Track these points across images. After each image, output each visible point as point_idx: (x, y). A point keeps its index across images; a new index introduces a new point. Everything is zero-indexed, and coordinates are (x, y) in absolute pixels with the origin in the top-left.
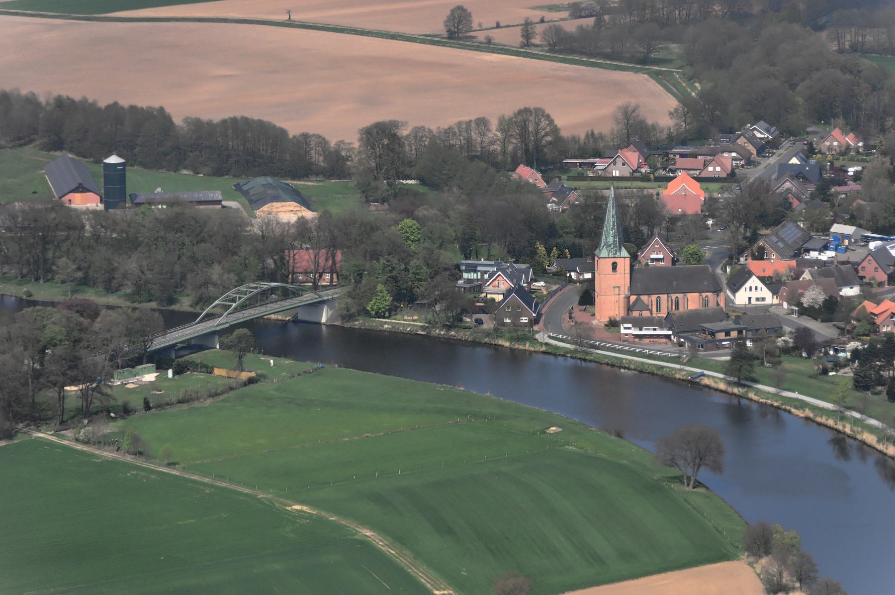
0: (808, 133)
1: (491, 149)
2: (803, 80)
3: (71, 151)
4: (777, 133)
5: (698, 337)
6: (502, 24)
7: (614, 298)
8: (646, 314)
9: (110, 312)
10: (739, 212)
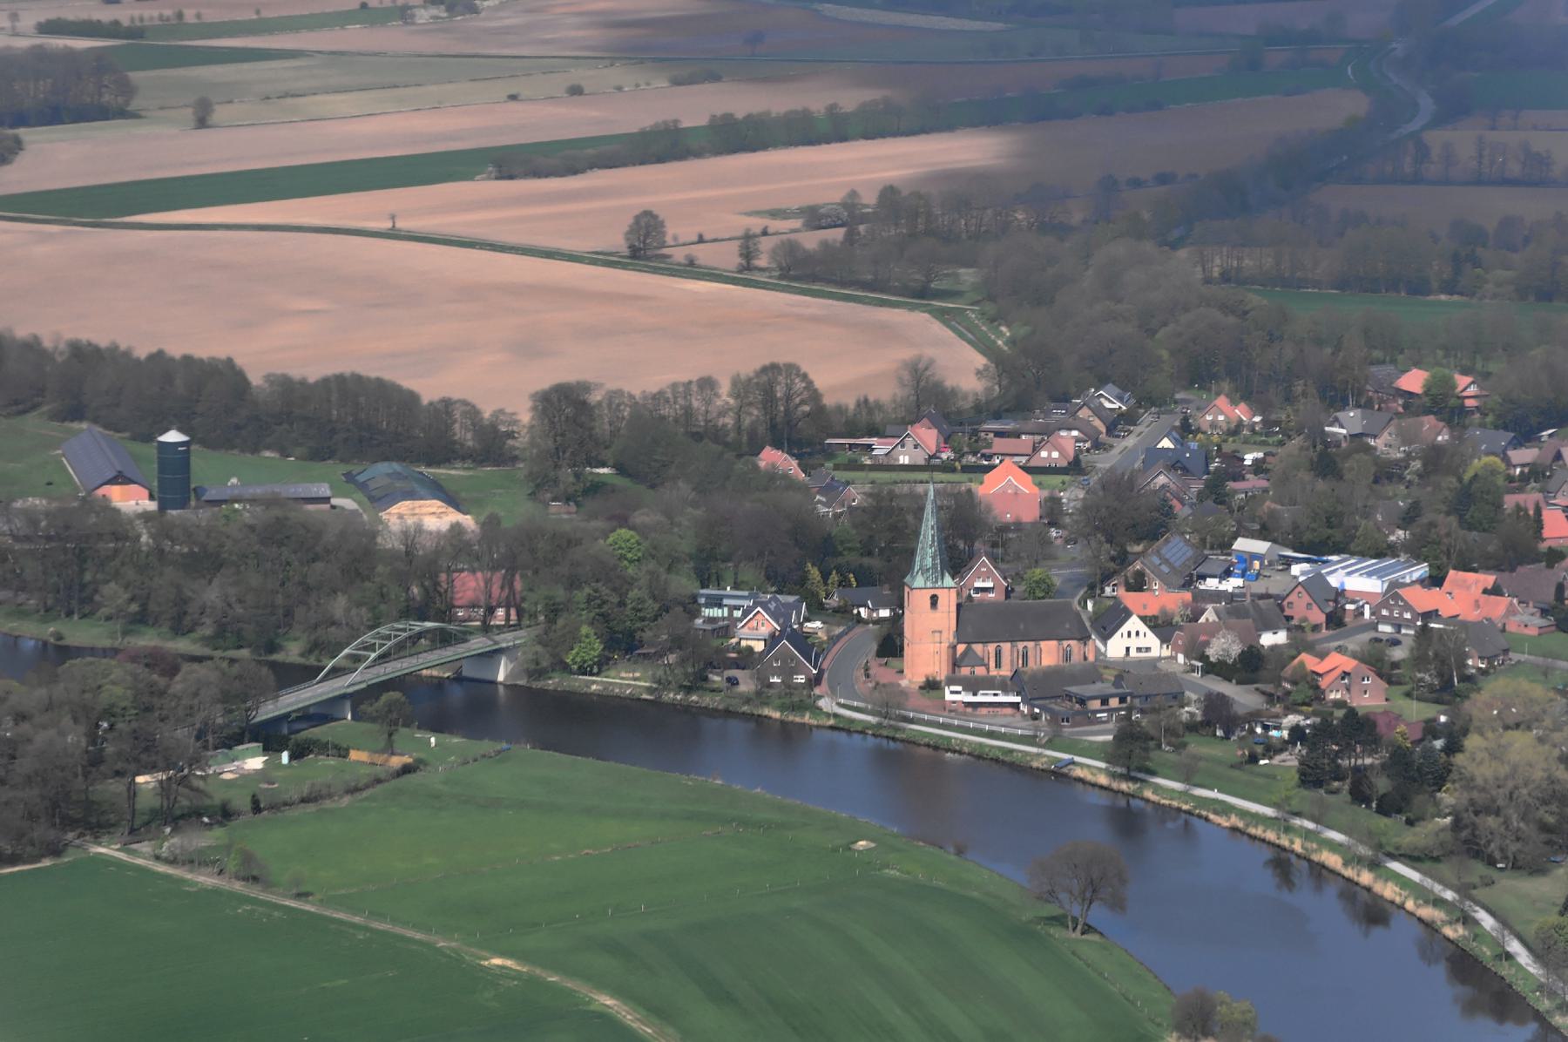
0: (1176, 402)
1: (720, 423)
2: (1165, 324)
3: (95, 421)
4: (1133, 401)
5: (1061, 707)
6: (707, 237)
7: (932, 648)
8: (980, 671)
9: (196, 666)
10: (1101, 520)
